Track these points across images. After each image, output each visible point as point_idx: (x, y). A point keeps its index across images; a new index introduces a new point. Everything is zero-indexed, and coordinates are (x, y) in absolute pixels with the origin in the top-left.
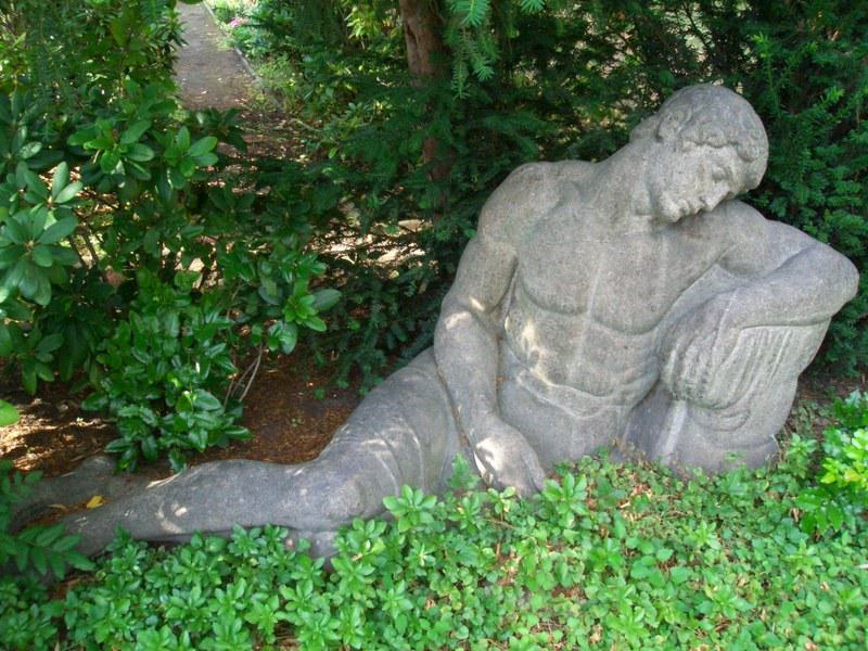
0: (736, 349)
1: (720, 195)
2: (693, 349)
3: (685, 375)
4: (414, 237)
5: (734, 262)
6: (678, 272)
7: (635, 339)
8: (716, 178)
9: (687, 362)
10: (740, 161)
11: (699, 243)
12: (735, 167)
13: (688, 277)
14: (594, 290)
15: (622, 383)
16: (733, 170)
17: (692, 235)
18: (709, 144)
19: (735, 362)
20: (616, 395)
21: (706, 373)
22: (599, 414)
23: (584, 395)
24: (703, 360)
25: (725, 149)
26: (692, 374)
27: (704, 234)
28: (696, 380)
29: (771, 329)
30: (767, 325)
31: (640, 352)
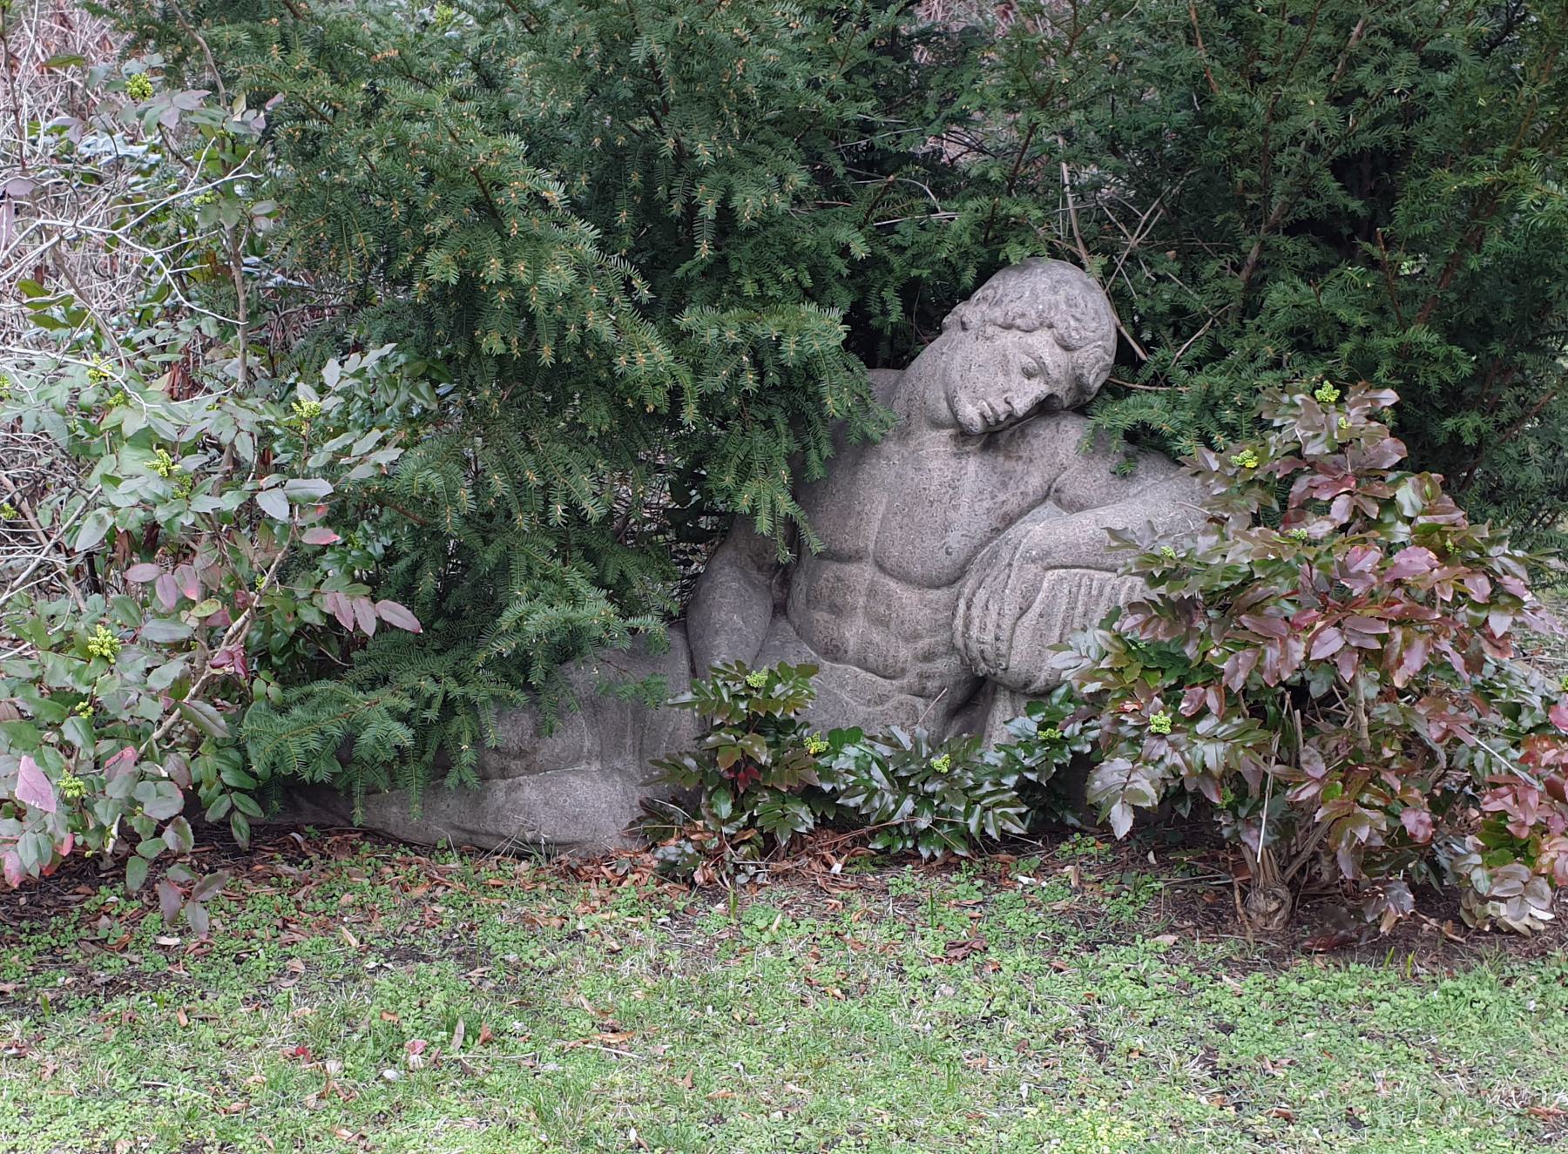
0: (1041, 596)
1: (1033, 396)
2: (982, 594)
3: (974, 632)
4: (1093, 758)
5: (1066, 497)
6: (986, 504)
7: (933, 595)
8: (1029, 375)
9: (976, 612)
10: (1058, 350)
11: (1020, 467)
12: (1052, 356)
13: (1001, 512)
14: (876, 526)
15: (916, 657)
16: (1048, 360)
17: (1008, 457)
18: (1018, 328)
19: (1041, 616)
20: (910, 679)
21: (999, 626)
22: (887, 705)
23: (869, 676)
24: (993, 608)
25: (1038, 332)
26: (983, 629)
27: (1025, 455)
28: (989, 638)
29: (1097, 575)
30: (1088, 567)
31: (939, 616)
